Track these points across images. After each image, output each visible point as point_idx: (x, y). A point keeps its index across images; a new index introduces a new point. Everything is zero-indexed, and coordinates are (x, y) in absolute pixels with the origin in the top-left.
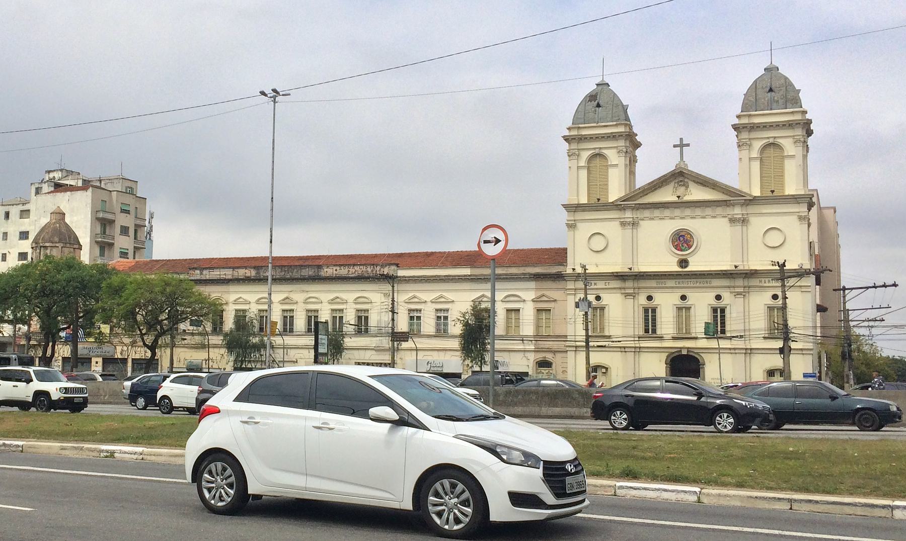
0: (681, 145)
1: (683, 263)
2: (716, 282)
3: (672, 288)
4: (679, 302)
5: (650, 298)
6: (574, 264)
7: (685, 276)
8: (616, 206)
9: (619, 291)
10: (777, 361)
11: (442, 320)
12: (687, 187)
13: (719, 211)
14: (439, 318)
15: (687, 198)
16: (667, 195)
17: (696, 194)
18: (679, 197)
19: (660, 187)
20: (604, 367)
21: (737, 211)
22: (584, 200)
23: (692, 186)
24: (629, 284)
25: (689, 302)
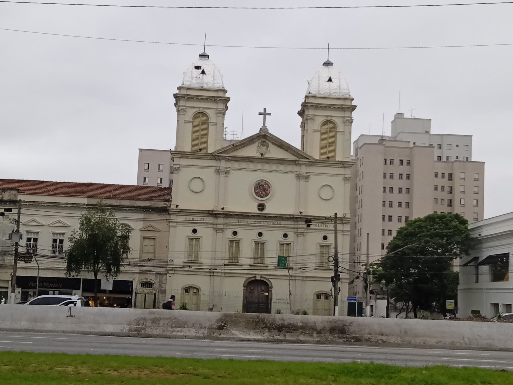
0: (265, 114)
1: (261, 207)
2: (284, 223)
3: (253, 226)
4: (191, 234)
5: (235, 233)
6: (181, 199)
7: (261, 216)
8: (214, 157)
9: (211, 226)
10: (328, 287)
11: (57, 243)
12: (268, 146)
13: (289, 168)
14: (55, 241)
15: (266, 156)
16: (252, 151)
17: (275, 153)
18: (262, 154)
19: (247, 145)
20: (195, 288)
21: (303, 170)
22: (188, 148)
23: (271, 146)
24: (220, 220)
25: (198, 234)
